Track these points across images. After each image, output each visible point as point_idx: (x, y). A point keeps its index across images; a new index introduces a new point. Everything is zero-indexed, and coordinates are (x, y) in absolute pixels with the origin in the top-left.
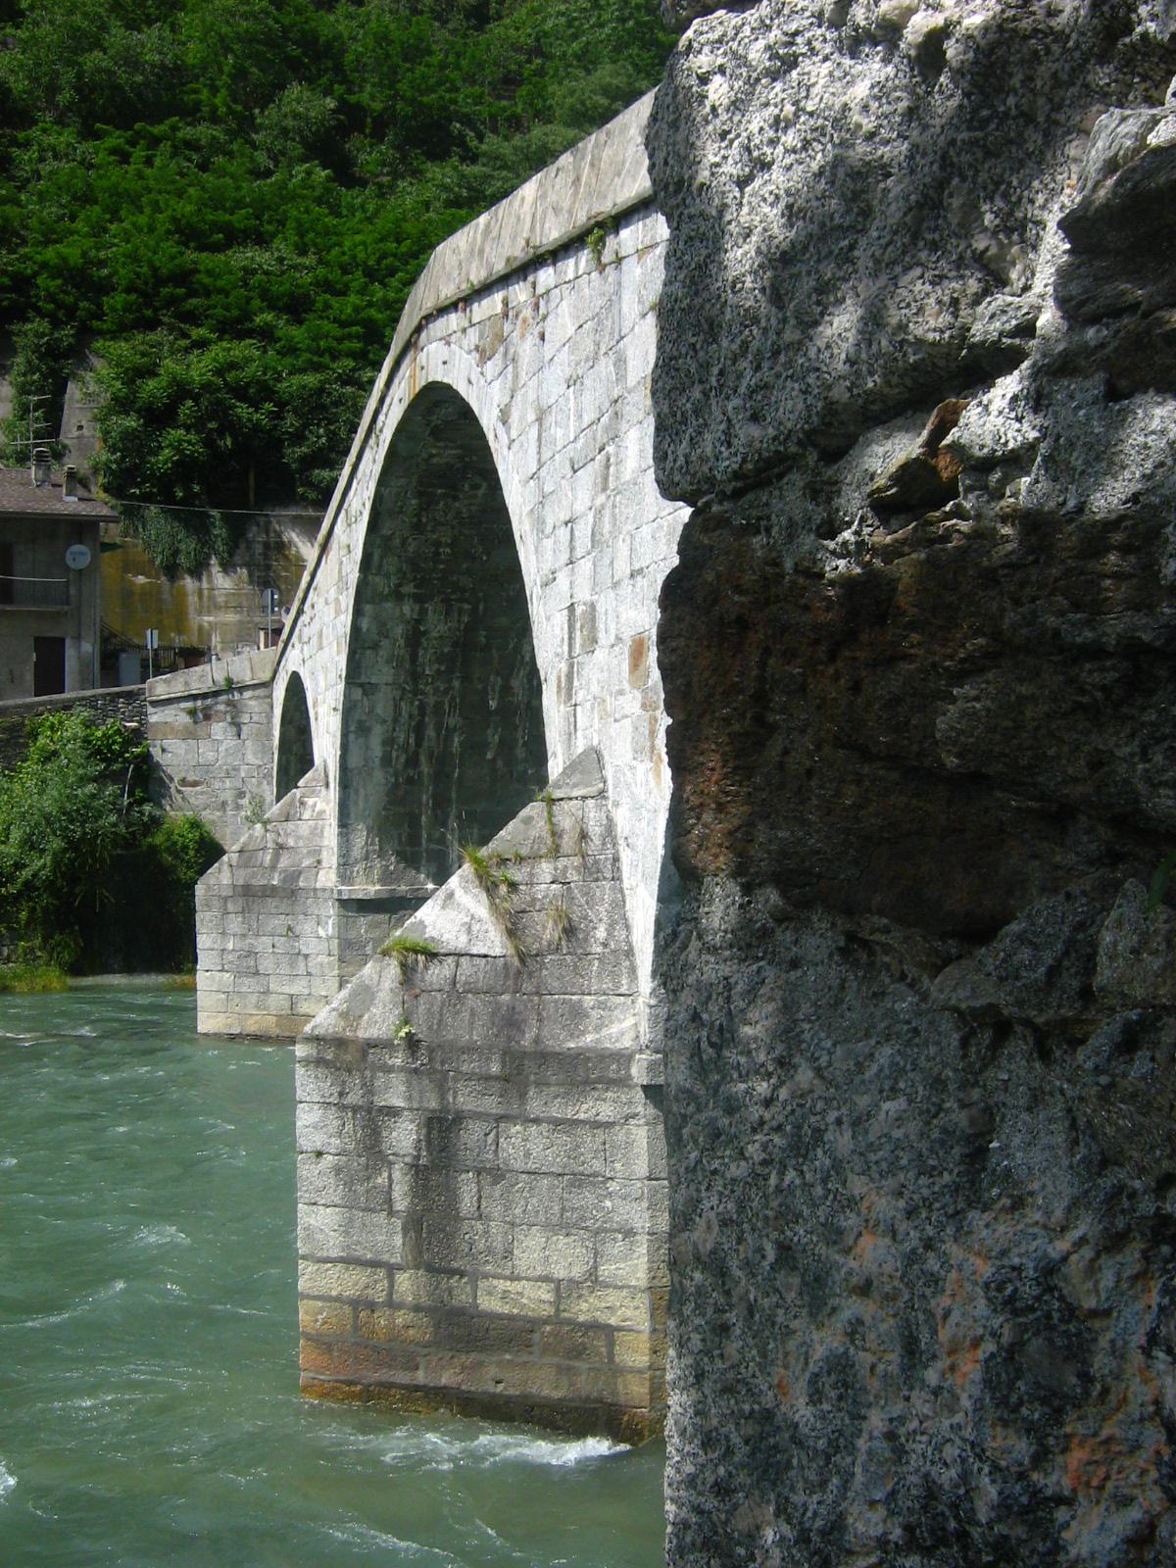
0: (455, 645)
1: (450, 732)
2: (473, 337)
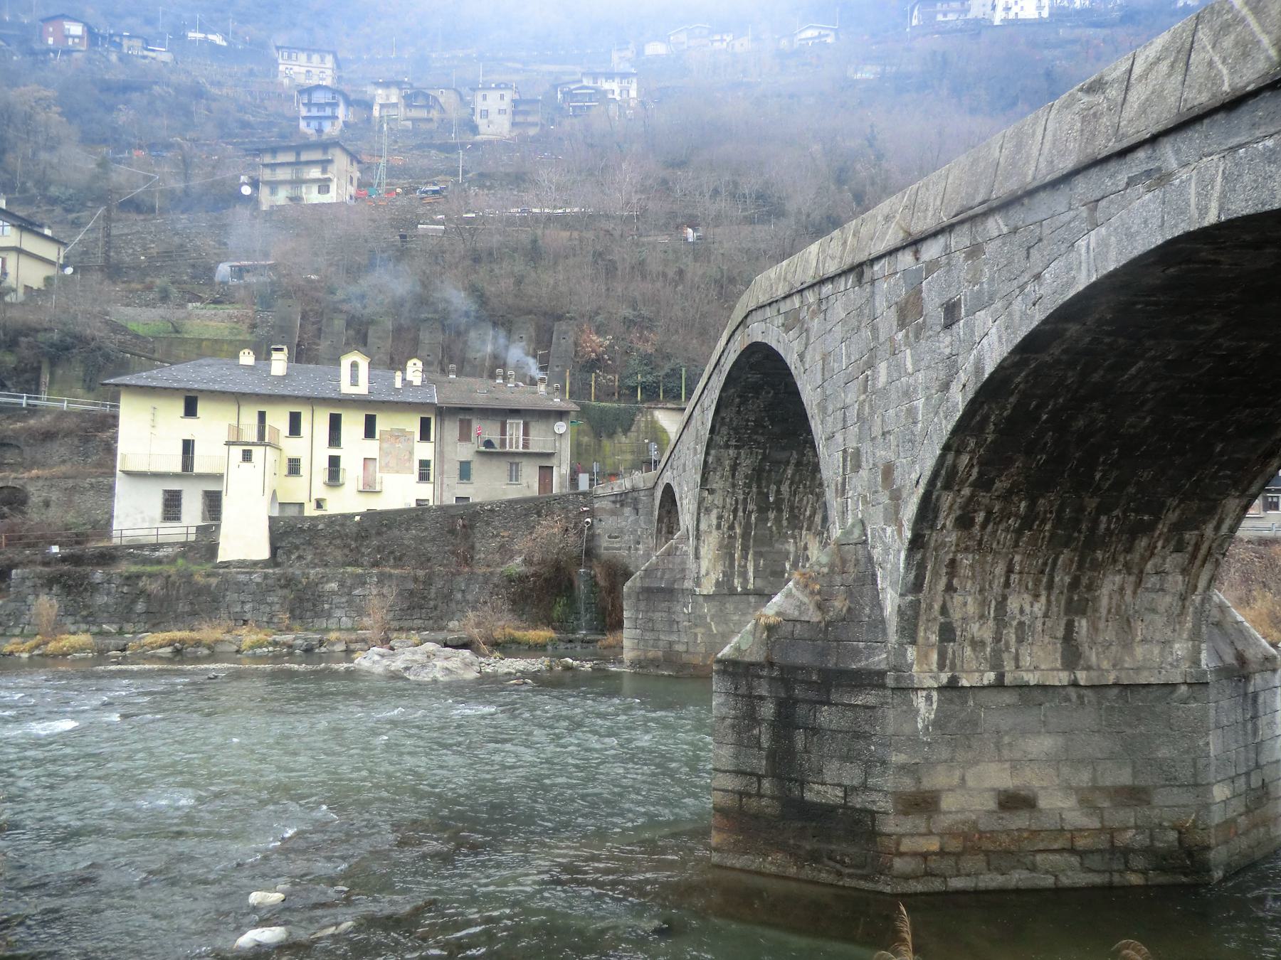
0: (753, 470)
1: (751, 513)
2: (780, 320)
